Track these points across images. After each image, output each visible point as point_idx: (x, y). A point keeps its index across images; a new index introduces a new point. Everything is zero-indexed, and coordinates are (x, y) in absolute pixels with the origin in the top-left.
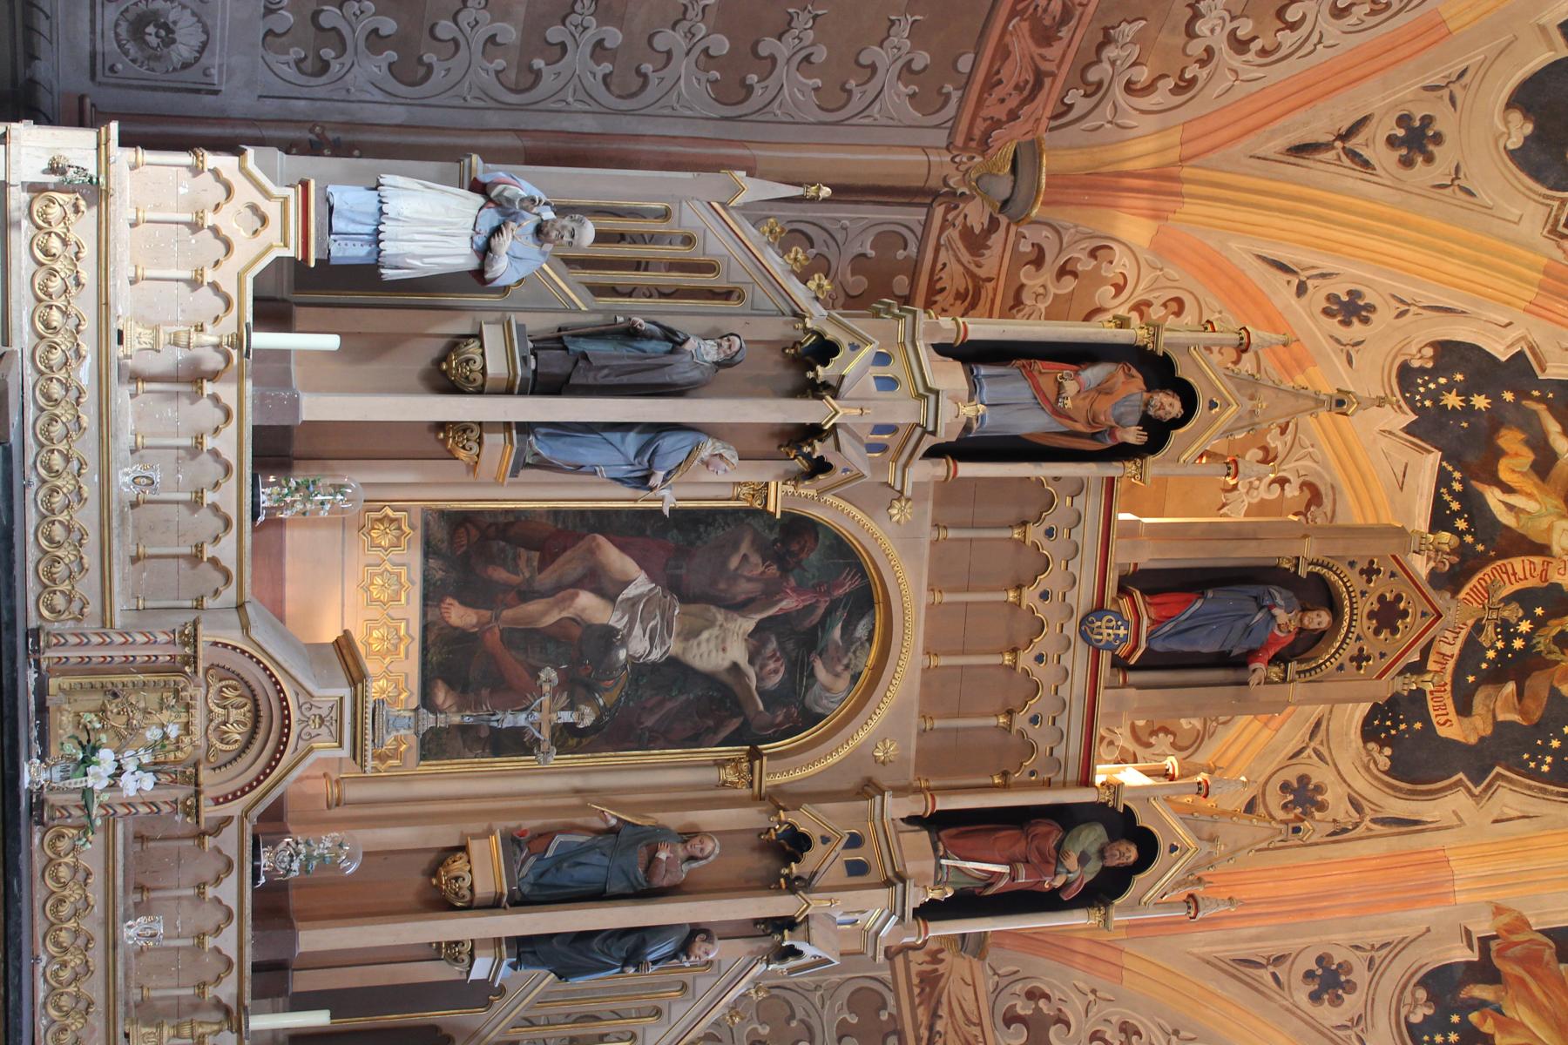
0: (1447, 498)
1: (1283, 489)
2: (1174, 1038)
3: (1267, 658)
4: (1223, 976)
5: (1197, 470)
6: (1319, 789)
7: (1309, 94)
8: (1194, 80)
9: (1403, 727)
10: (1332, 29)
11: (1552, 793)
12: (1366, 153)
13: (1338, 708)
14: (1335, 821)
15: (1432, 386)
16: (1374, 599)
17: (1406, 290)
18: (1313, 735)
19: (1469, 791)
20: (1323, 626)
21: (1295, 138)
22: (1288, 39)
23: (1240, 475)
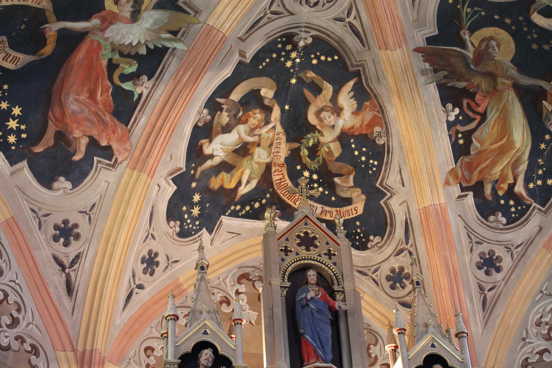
0: (244, 212)
1: (241, 293)
2: (527, 340)
3: (332, 301)
4: (492, 316)
5: (239, 339)
6: (393, 270)
7: (40, 286)
8: (32, 346)
9: (359, 230)
10: (8, 276)
11: (388, 160)
12: (72, 257)
13: (354, 264)
14: (411, 264)
15: (189, 221)
16: (300, 249)
17: (142, 235)
18: (365, 274)
19: (389, 198)
20: (315, 273)
21: (63, 292)
22: (12, 298)
23: (241, 318)
